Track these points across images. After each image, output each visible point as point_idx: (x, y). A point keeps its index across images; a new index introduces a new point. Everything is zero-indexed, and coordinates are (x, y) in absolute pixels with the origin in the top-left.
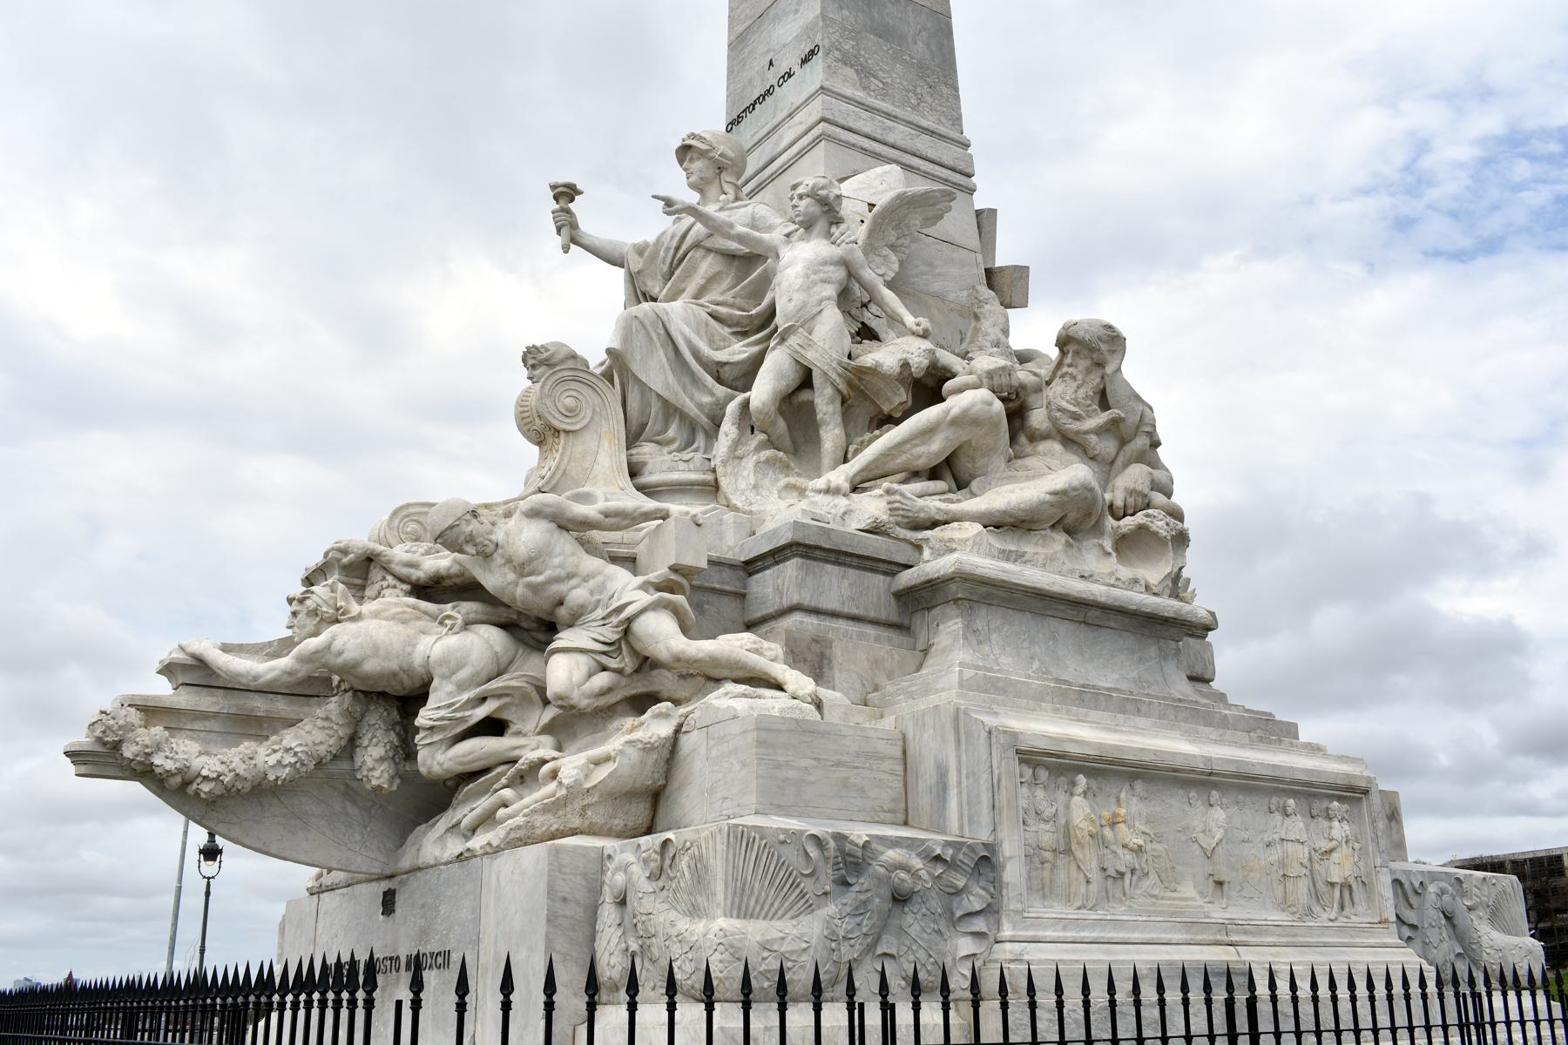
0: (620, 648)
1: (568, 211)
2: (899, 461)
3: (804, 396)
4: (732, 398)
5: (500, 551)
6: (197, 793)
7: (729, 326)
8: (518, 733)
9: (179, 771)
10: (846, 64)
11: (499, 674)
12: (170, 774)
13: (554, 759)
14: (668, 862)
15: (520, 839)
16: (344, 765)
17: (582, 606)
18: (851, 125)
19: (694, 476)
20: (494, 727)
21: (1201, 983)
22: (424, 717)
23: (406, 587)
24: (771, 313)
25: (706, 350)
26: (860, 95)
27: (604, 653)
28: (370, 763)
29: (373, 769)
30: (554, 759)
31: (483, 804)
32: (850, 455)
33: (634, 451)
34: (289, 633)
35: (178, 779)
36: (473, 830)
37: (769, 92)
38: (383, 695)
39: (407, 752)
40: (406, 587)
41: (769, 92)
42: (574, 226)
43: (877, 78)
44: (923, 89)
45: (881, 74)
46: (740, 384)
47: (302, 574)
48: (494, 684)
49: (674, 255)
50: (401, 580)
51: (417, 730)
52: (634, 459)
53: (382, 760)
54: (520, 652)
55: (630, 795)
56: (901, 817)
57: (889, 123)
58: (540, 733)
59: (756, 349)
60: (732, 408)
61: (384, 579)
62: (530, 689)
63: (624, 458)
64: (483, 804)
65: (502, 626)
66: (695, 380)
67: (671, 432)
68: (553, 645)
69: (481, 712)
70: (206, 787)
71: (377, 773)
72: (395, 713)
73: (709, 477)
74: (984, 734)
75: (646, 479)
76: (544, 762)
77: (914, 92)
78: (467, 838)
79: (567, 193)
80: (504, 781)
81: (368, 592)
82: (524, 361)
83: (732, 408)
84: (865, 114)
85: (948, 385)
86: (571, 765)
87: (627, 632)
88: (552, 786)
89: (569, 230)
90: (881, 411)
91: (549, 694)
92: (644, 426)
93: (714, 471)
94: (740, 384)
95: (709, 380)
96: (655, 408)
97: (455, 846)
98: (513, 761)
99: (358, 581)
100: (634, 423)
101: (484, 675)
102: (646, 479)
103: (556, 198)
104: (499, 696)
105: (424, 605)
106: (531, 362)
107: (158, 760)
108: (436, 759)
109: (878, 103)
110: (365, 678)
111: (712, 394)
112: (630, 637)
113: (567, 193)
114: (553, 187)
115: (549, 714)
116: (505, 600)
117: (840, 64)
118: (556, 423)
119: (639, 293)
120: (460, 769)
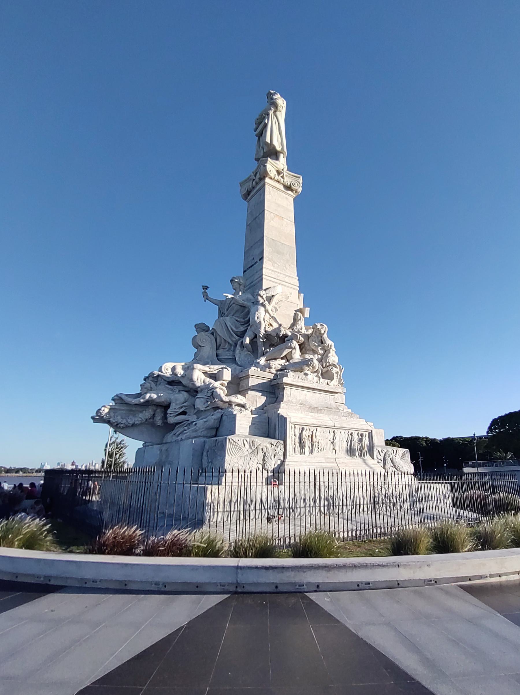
0: (211, 397)
1: (206, 292)
2: (19, 593)
3: (255, 340)
4: (240, 340)
5: (186, 376)
6: (120, 427)
7: (240, 322)
8: (189, 415)
9: (116, 422)
10: (269, 261)
11: (186, 402)
12: (114, 423)
13: (196, 421)
14: (217, 444)
15: (188, 438)
16: (151, 420)
17: (203, 388)
18: (270, 276)
19: (230, 357)
20: (184, 413)
21: (390, 473)
22: (169, 411)
23: (166, 382)
24: (249, 320)
25: (234, 329)
26: (272, 268)
27: (208, 398)
28: (157, 420)
29: (158, 421)
30: (196, 421)
31: (181, 430)
32: (265, 353)
33: (218, 351)
34: (141, 392)
35: (116, 424)
36: (179, 435)
37: (252, 266)
38: (161, 406)
39: (165, 417)
40: (166, 382)
41: (252, 266)
42: (207, 296)
43: (277, 264)
44: (287, 266)
45: (277, 263)
46: (242, 336)
47: (143, 378)
48: (183, 405)
49: (229, 305)
50: (165, 381)
51: (167, 414)
52: (218, 353)
53: (160, 419)
54: (190, 397)
55: (211, 428)
56: (267, 435)
57: (279, 275)
58: (194, 415)
59: (245, 328)
60: (239, 343)
61: (161, 380)
62: (192, 405)
63: (215, 352)
64: (181, 430)
65: (186, 391)
66: (232, 335)
67: (226, 347)
68: (197, 396)
69: (181, 410)
70: (122, 425)
71: (158, 422)
72: (163, 409)
73: (234, 357)
74: (284, 419)
75: (219, 358)
76: (194, 421)
77: (285, 267)
78: (177, 437)
79: (206, 288)
80: (185, 425)
81: (158, 383)
82: (195, 326)
83: (239, 343)
84: (273, 273)
85: (286, 339)
86: (200, 422)
87: (212, 394)
88: (195, 427)
89: (206, 297)
90: (272, 344)
91: (196, 407)
92: (220, 345)
93: (235, 356)
94: (242, 336)
95: (235, 335)
96: (223, 341)
97: (175, 438)
98: (188, 420)
99: (156, 380)
100: (218, 344)
101: (182, 402)
102: (219, 358)
103: (203, 289)
104: (185, 407)
105: (170, 387)
106: (196, 327)
107: (111, 419)
108: (171, 420)
109: (277, 270)
110: (157, 402)
111: (236, 338)
112: (213, 395)
113: (206, 288)
114: (203, 286)
115: (196, 411)
116: (187, 386)
117: (268, 261)
118: (200, 344)
119: (221, 314)
120: (176, 422)
